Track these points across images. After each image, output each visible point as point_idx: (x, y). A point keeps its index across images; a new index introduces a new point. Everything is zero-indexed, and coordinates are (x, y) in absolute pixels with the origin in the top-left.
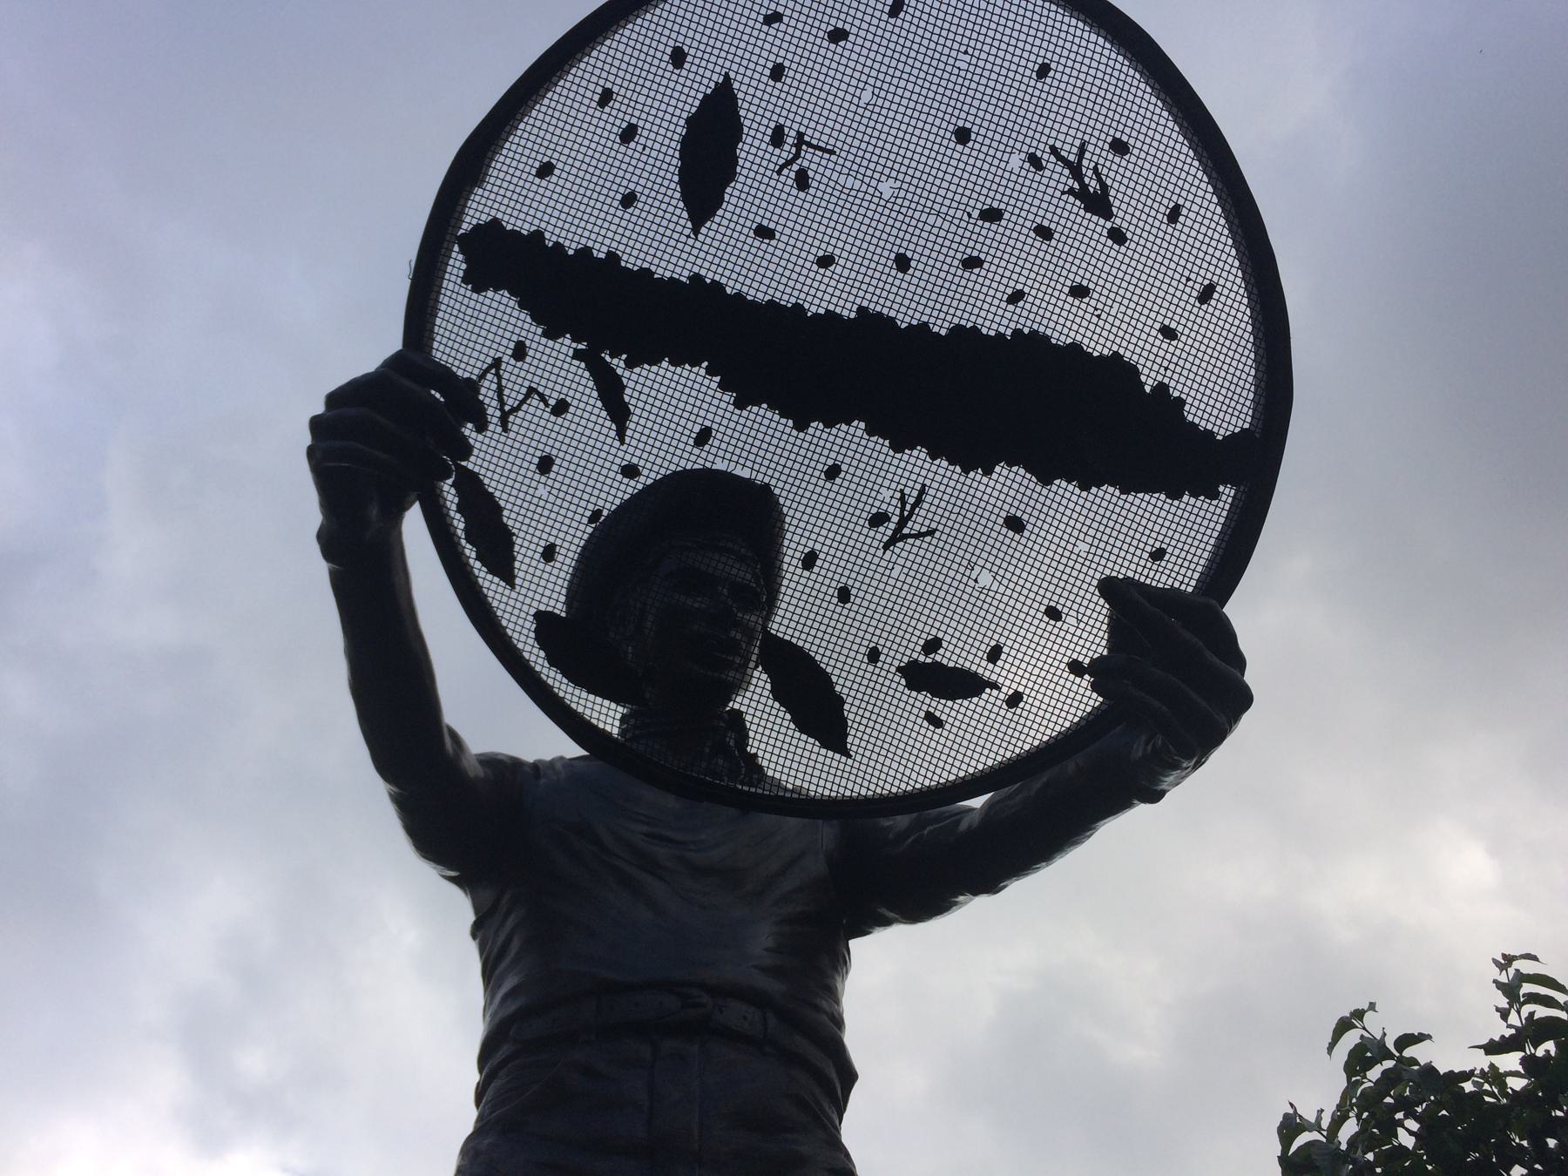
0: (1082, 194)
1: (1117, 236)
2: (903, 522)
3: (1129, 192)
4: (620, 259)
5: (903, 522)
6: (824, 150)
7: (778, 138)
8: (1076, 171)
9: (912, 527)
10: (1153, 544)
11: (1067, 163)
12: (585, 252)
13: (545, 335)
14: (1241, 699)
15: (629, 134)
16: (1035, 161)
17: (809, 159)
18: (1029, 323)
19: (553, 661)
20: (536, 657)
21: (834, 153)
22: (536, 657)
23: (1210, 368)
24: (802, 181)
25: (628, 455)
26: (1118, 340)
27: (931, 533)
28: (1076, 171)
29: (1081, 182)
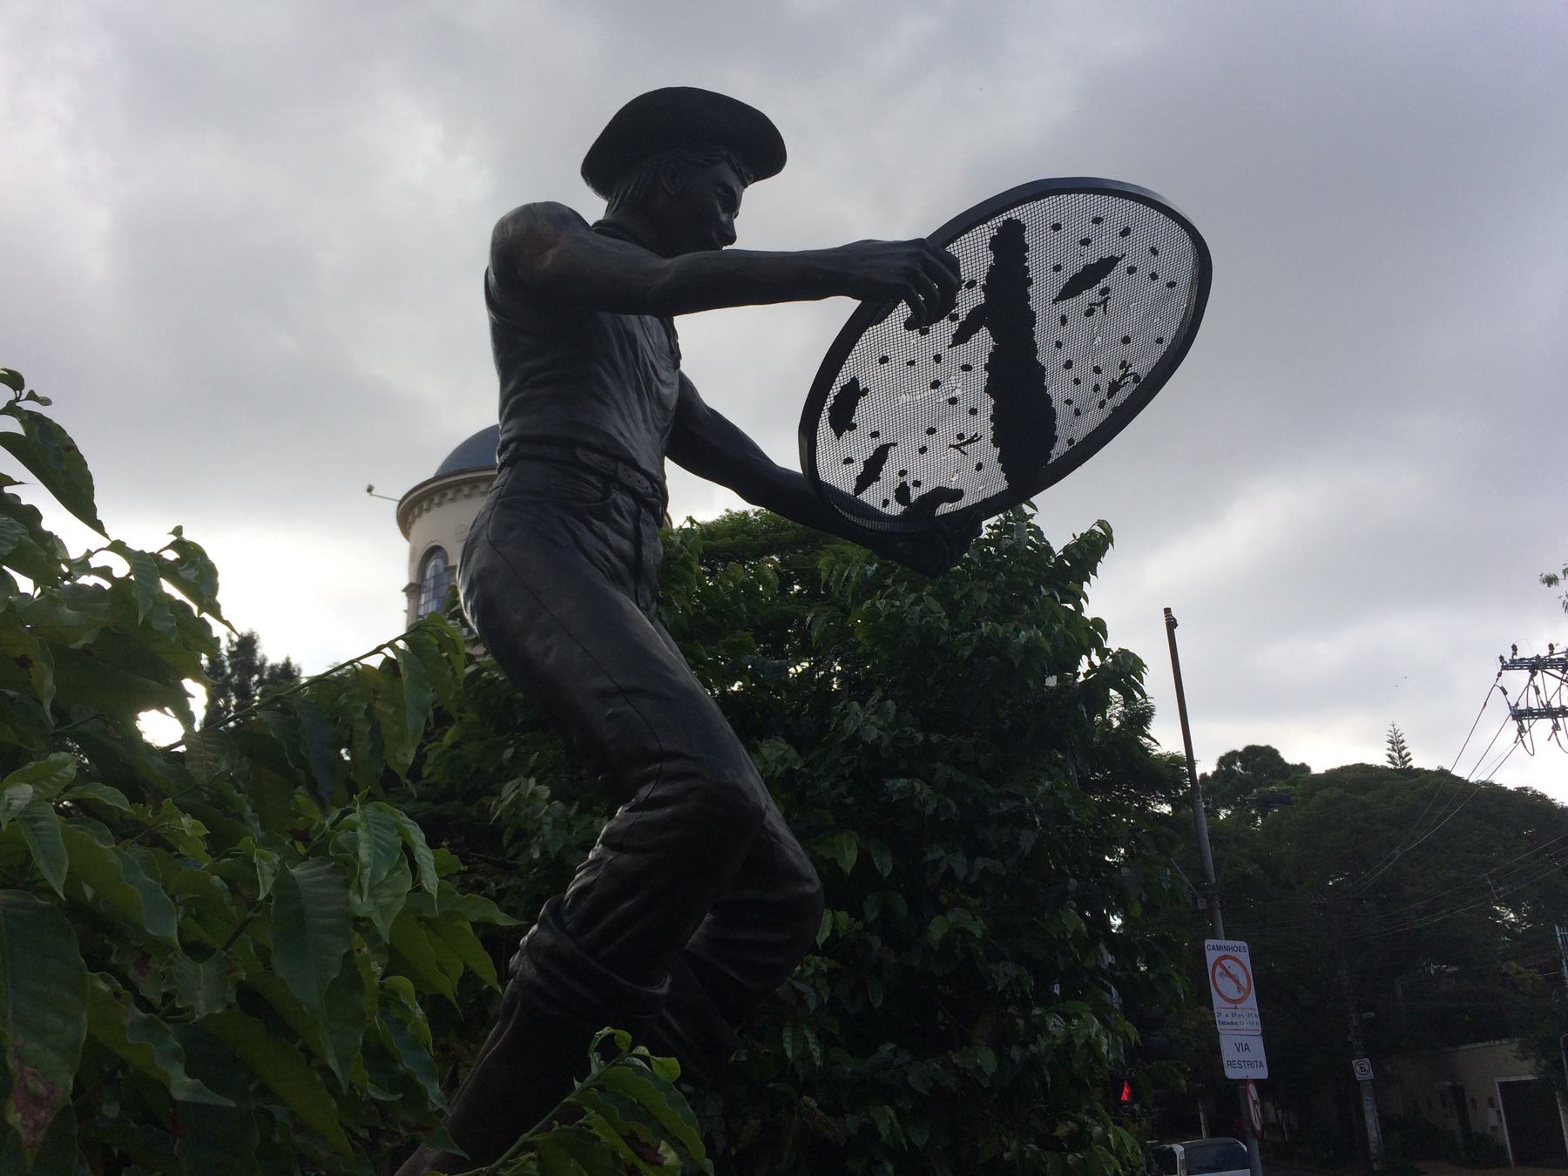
2: (964, 444)
5: (964, 444)
7: (1105, 291)
12: (1027, 270)
15: (1085, 242)
17: (1099, 310)
20: (835, 390)
22: (835, 390)
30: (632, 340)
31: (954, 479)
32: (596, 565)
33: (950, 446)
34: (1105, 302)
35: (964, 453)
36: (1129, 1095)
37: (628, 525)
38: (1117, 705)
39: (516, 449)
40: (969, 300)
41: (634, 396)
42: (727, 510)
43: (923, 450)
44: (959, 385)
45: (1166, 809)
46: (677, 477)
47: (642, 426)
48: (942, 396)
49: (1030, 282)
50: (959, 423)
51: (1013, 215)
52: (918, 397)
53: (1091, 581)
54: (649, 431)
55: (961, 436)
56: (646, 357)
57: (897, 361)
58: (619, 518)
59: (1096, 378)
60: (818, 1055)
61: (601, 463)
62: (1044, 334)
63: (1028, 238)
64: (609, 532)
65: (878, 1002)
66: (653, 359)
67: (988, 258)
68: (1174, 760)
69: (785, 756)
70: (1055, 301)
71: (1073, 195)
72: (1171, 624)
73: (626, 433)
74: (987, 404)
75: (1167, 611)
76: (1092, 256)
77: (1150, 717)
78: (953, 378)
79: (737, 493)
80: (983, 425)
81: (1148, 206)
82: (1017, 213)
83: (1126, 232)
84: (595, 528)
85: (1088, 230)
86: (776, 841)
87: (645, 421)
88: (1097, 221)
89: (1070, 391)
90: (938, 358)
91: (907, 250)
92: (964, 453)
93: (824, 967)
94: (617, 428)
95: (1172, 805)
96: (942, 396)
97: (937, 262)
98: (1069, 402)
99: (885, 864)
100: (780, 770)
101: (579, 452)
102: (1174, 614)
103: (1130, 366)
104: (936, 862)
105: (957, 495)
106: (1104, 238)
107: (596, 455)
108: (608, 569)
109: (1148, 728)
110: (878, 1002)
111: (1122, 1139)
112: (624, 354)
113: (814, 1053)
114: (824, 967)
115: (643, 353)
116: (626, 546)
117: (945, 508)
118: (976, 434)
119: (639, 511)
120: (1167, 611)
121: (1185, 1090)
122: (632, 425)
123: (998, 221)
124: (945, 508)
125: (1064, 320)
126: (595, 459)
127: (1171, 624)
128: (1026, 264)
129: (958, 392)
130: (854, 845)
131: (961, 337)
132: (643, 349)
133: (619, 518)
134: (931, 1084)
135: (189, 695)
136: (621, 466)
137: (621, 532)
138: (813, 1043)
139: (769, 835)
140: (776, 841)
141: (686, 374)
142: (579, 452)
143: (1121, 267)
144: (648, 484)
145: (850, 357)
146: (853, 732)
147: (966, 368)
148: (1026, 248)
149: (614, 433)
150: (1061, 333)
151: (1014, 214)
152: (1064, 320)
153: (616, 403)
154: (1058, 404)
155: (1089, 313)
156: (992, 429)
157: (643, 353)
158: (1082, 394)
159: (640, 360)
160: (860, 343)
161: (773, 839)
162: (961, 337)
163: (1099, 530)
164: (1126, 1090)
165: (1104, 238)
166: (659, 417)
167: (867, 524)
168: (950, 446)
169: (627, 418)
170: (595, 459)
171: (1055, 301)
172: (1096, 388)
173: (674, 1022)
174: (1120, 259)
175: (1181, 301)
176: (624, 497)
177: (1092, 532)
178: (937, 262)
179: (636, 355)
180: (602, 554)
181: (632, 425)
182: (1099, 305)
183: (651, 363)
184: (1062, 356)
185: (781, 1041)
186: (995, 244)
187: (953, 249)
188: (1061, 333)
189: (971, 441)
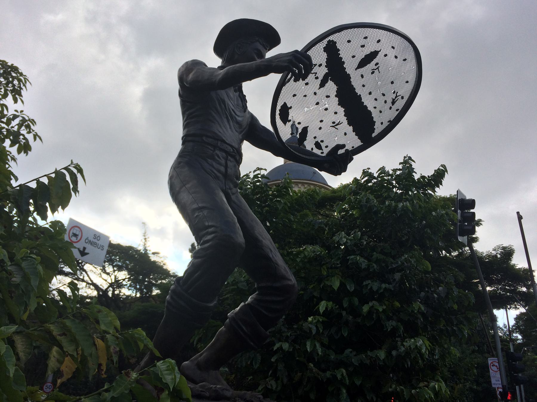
0: (393, 100)
1: (391, 108)
2: (336, 125)
3: (314, 52)
4: (344, 64)
5: (336, 125)
6: (379, 72)
7: (377, 64)
8: (396, 97)
9: (336, 127)
10: (347, 133)
11: (396, 95)
12: (341, 58)
13: (325, 66)
14: (345, 170)
15: (363, 46)
16: (394, 92)
17: (376, 71)
18: (325, 69)
19: (280, 110)
20: (278, 108)
21: (379, 73)
22: (278, 108)
23: (323, 71)
24: (373, 73)
25: (317, 91)
26: (324, 68)
27: (337, 129)
28: (396, 97)
29: (395, 98)
30: (224, 102)
31: (336, 139)
32: (208, 174)
33: (331, 127)
34: (378, 68)
35: (336, 129)
36: (511, 397)
37: (223, 162)
38: (499, 249)
39: (185, 138)
40: (322, 71)
41: (225, 120)
42: (341, 184)
43: (320, 128)
44: (326, 103)
45: (524, 289)
46: (247, 147)
47: (229, 129)
48: (321, 108)
49: (344, 63)
50: (330, 118)
51: (330, 38)
52: (311, 108)
53: (440, 187)
54: (232, 131)
55: (334, 123)
56: (230, 108)
57: (300, 96)
58: (218, 159)
59: (384, 98)
60: (320, 351)
61: (212, 141)
62: (356, 82)
63: (338, 46)
64: (214, 164)
65: (345, 335)
66: (233, 108)
67: (325, 56)
68: (525, 270)
69: (314, 250)
70: (356, 69)
71: (352, 29)
72: (520, 218)
73: (221, 131)
74: (341, 111)
75: (518, 213)
76: (367, 51)
77: (513, 253)
78: (323, 100)
79: (271, 153)
80: (341, 117)
81: (385, 30)
82: (331, 38)
83: (379, 41)
84: (209, 162)
85: (363, 42)
86: (277, 266)
87: (230, 128)
88: (366, 38)
89: (375, 103)
90: (315, 94)
91: (291, 54)
92: (336, 129)
93: (321, 320)
94: (218, 130)
95: (526, 288)
96: (321, 108)
97: (302, 58)
98: (375, 108)
99: (351, 287)
100: (313, 254)
101: (204, 138)
102: (521, 214)
103: (398, 92)
104: (367, 285)
105: (343, 146)
106: (370, 44)
107: (211, 139)
108: (213, 175)
109: (512, 258)
110: (345, 335)
111: (441, 387)
112: (220, 105)
113: (319, 350)
114: (321, 320)
115: (228, 106)
116: (222, 169)
117: (341, 152)
118: (340, 122)
119: (227, 157)
120: (518, 213)
121: (476, 374)
122: (225, 130)
123: (325, 42)
124: (341, 152)
125: (362, 76)
126: (210, 140)
127: (520, 218)
128: (340, 56)
129: (327, 106)
130: (339, 281)
131: (322, 85)
132: (228, 104)
133: (218, 159)
134: (360, 362)
135: (58, 210)
136: (219, 143)
137: (220, 164)
138: (319, 347)
139: (275, 264)
140: (277, 266)
141: (254, 114)
142: (204, 138)
143: (380, 55)
144: (231, 148)
145: (281, 95)
146: (337, 241)
147: (328, 97)
148: (339, 50)
149: (218, 132)
150: (363, 81)
151: (331, 38)
152: (362, 76)
153: (218, 122)
154: (370, 108)
155: (373, 73)
156: (347, 119)
157: (228, 106)
158: (380, 104)
159: (227, 109)
160: (283, 90)
161: (276, 265)
162: (322, 85)
163: (441, 168)
164: (509, 395)
165: (370, 44)
166: (237, 127)
167: (313, 158)
168: (331, 127)
169: (223, 127)
170: (210, 140)
171: (356, 69)
172: (386, 102)
173: (244, 328)
174: (380, 51)
175: (412, 64)
176: (221, 153)
177: (439, 169)
178: (302, 58)
179: (225, 106)
180: (211, 170)
181: (225, 130)
182: (376, 69)
183: (233, 110)
184: (366, 90)
185: (305, 345)
186: (326, 49)
187: (309, 53)
188: (363, 81)
189: (337, 125)
